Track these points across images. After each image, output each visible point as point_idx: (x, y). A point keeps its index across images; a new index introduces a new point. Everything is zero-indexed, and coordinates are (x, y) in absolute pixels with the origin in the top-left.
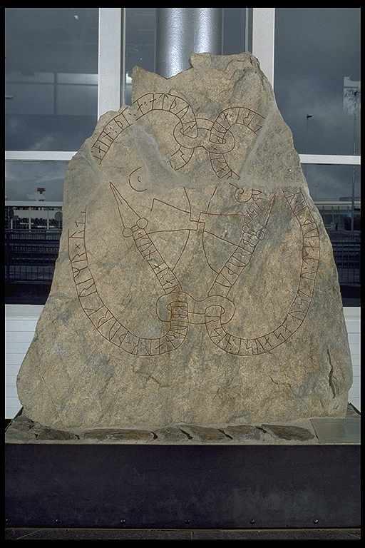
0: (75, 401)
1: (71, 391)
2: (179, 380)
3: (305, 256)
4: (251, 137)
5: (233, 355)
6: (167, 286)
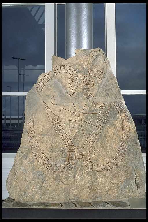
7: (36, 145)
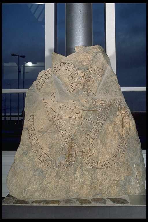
4: (100, 79)
5: (95, 169)
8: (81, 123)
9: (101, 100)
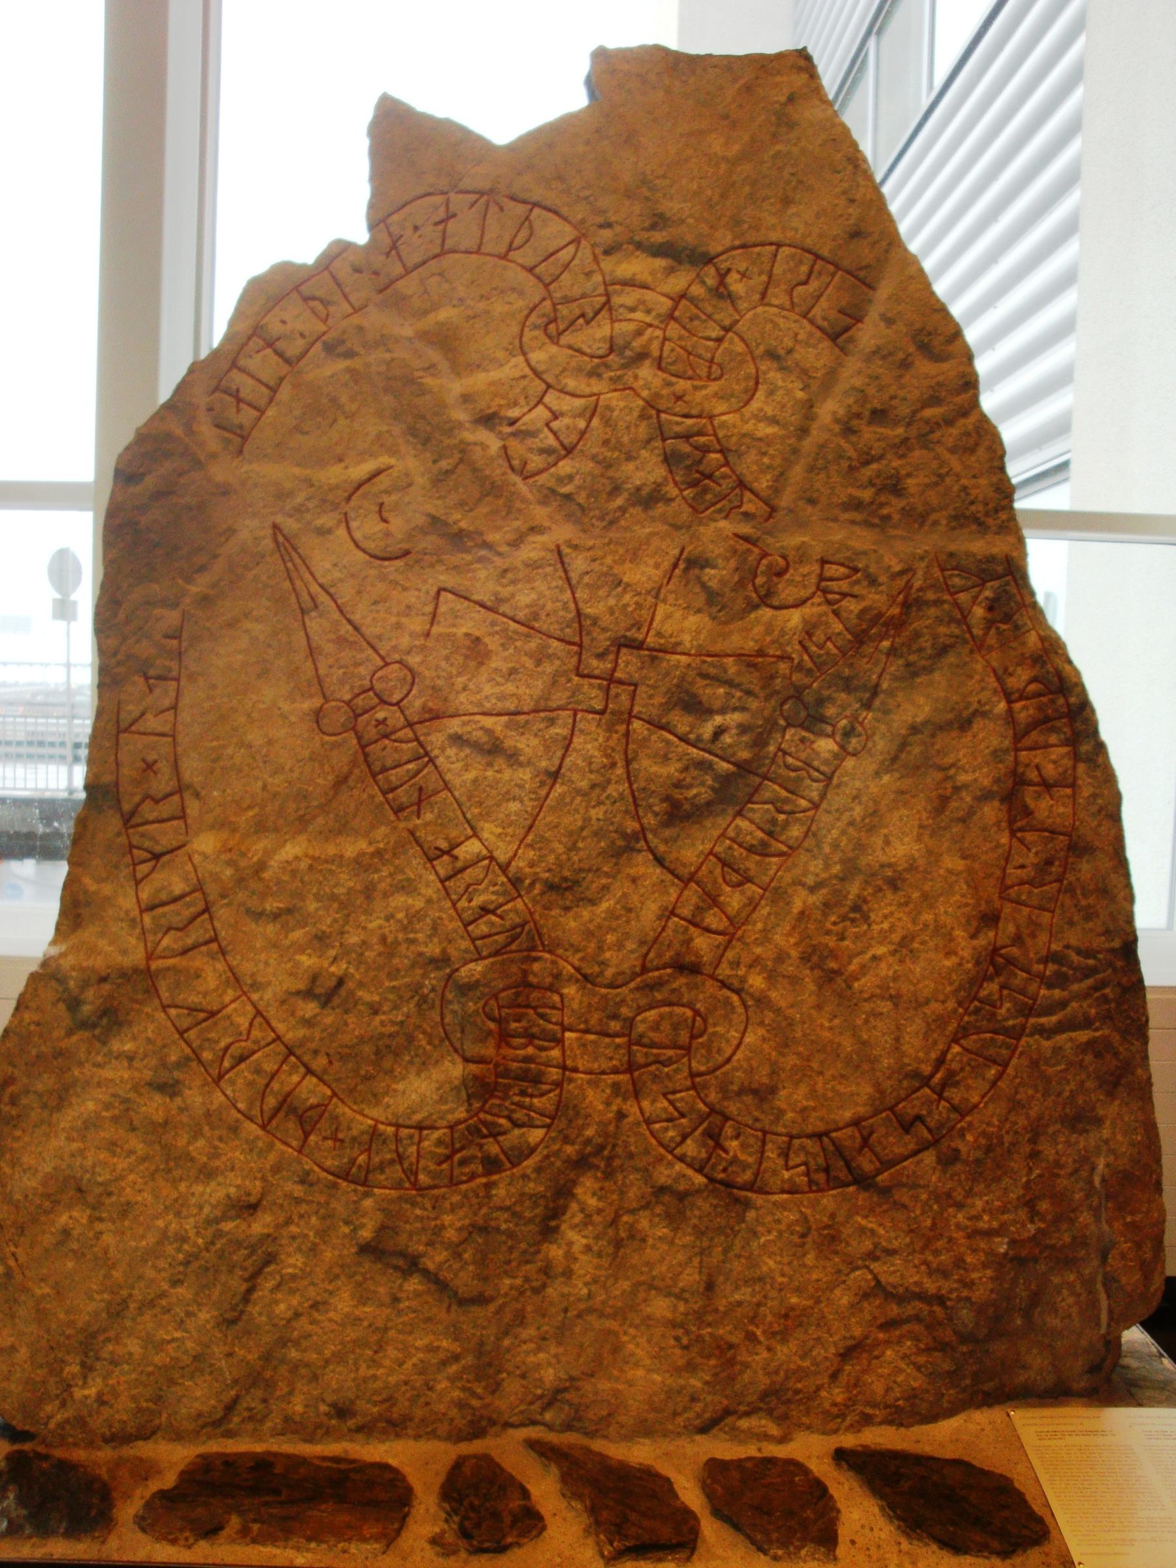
0: (134, 1346)
1: (117, 1311)
2: (527, 1279)
3: (1017, 815)
4: (816, 355)
5: (732, 1192)
6: (482, 928)
7: (196, 934)
8: (620, 771)
9: (823, 562)
